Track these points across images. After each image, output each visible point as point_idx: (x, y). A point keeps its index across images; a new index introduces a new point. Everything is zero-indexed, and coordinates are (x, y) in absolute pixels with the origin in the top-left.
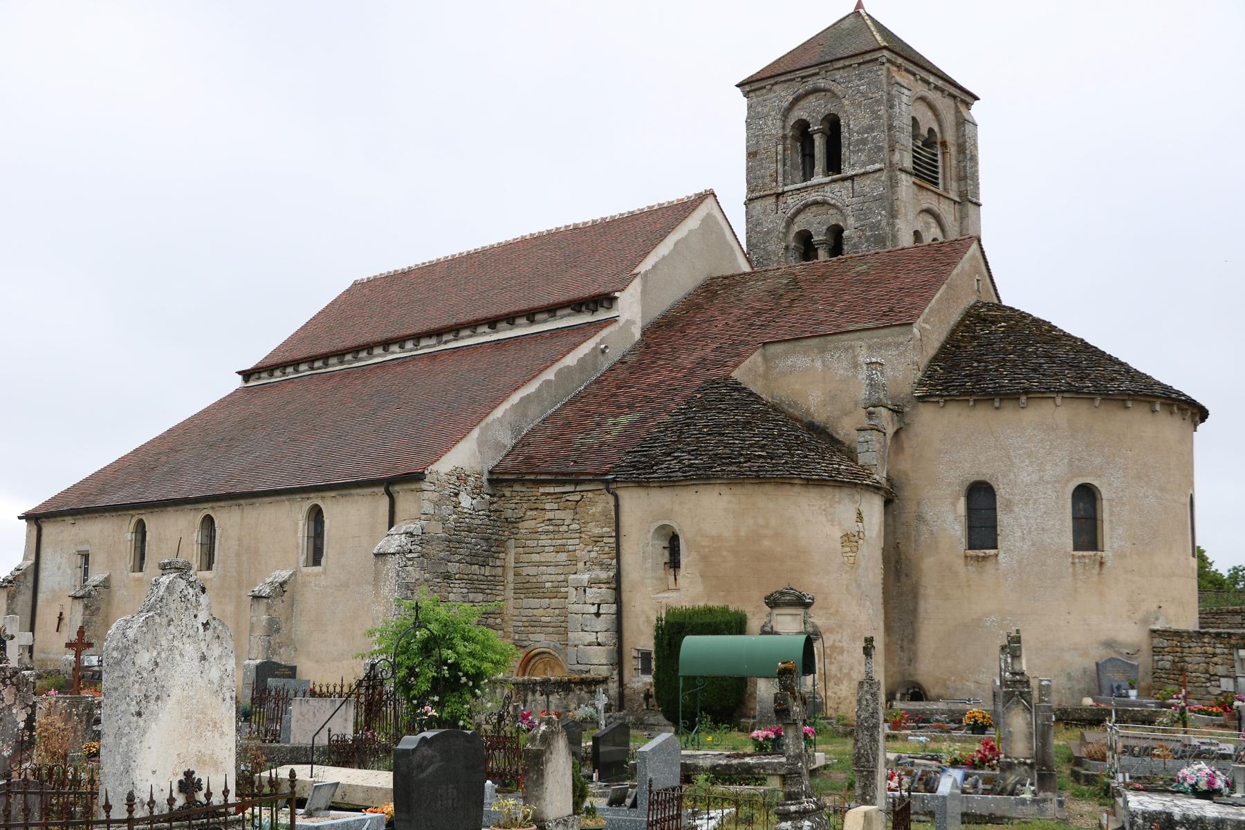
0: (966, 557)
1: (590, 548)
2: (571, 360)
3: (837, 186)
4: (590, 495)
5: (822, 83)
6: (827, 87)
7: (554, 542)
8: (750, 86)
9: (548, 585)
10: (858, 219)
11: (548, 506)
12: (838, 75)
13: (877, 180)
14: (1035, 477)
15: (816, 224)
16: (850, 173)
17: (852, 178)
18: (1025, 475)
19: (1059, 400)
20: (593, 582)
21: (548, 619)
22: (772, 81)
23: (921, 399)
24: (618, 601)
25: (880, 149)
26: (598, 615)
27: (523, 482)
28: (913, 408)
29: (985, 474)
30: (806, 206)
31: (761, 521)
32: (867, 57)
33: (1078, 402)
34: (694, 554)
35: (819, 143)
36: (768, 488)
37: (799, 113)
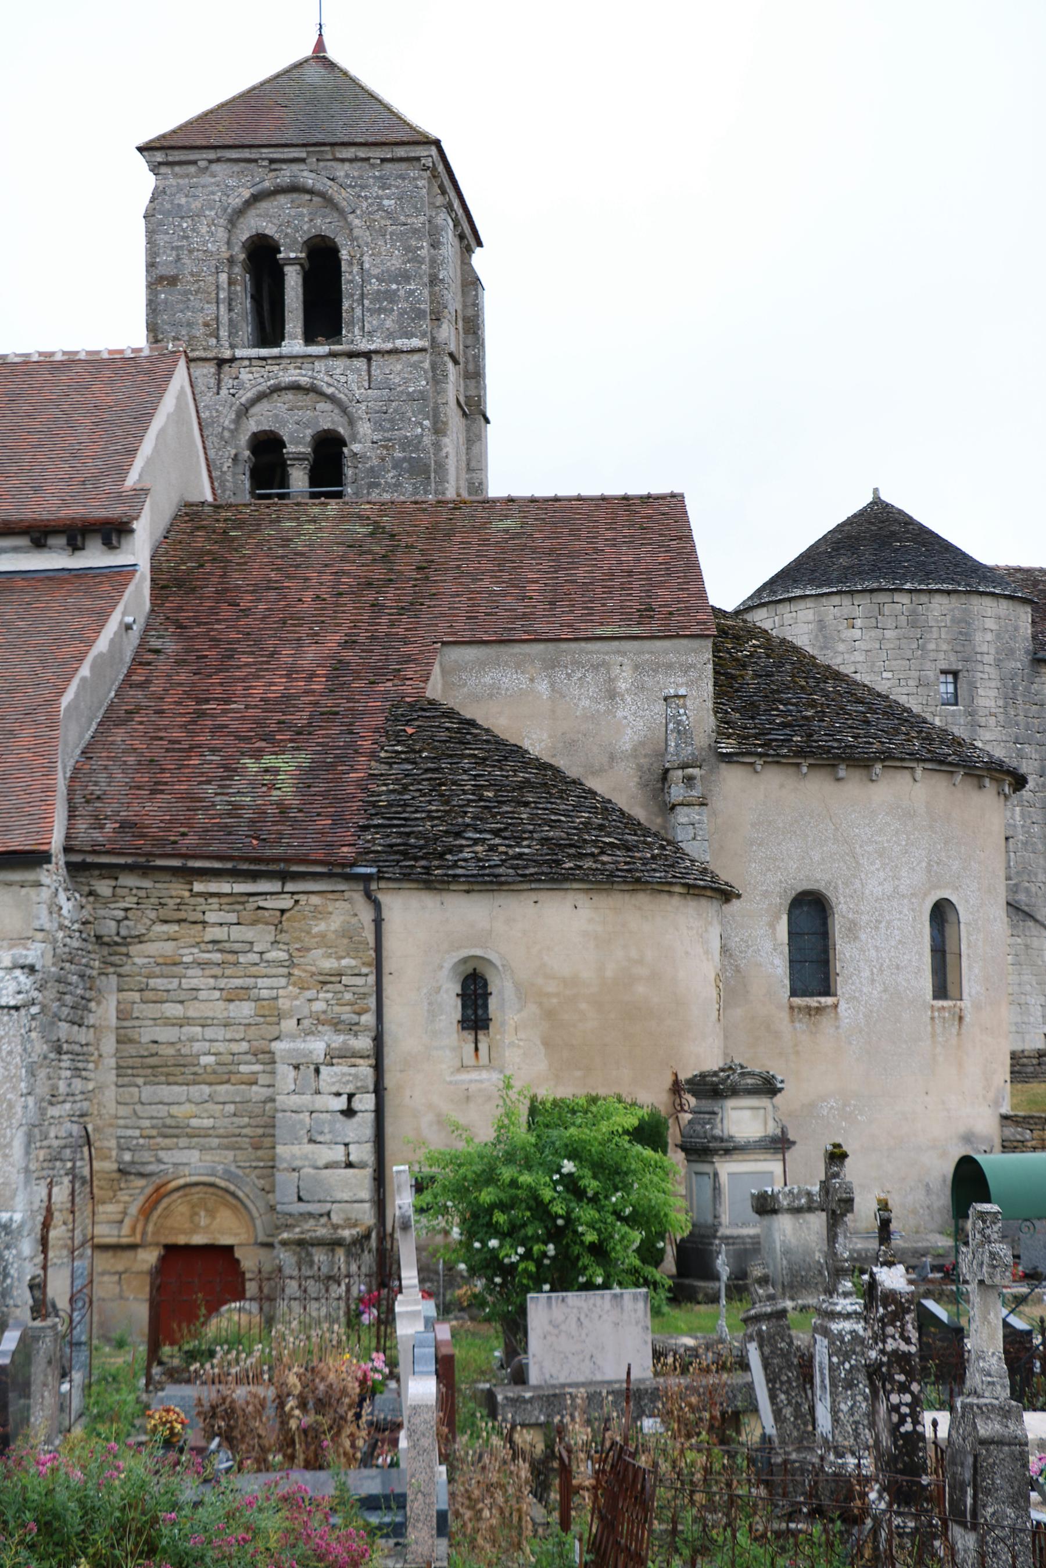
0: (792, 1008)
1: (310, 994)
2: (102, 644)
3: (340, 364)
4: (315, 900)
5: (309, 179)
6: (319, 187)
7: (222, 983)
8: (163, 152)
9: (205, 1060)
10: (378, 427)
11: (211, 917)
12: (341, 171)
13: (415, 366)
14: (888, 888)
15: (297, 428)
16: (364, 346)
17: (368, 355)
18: (875, 883)
19: (919, 772)
20: (332, 1057)
22: (212, 155)
23: (727, 758)
24: (379, 1090)
25: (420, 314)
26: (349, 1112)
27: (144, 870)
28: (711, 771)
29: (816, 879)
30: (277, 389)
31: (634, 954)
32: (401, 152)
33: (937, 775)
34: (532, 1008)
35: (293, 281)
36: (643, 899)
37: (256, 223)
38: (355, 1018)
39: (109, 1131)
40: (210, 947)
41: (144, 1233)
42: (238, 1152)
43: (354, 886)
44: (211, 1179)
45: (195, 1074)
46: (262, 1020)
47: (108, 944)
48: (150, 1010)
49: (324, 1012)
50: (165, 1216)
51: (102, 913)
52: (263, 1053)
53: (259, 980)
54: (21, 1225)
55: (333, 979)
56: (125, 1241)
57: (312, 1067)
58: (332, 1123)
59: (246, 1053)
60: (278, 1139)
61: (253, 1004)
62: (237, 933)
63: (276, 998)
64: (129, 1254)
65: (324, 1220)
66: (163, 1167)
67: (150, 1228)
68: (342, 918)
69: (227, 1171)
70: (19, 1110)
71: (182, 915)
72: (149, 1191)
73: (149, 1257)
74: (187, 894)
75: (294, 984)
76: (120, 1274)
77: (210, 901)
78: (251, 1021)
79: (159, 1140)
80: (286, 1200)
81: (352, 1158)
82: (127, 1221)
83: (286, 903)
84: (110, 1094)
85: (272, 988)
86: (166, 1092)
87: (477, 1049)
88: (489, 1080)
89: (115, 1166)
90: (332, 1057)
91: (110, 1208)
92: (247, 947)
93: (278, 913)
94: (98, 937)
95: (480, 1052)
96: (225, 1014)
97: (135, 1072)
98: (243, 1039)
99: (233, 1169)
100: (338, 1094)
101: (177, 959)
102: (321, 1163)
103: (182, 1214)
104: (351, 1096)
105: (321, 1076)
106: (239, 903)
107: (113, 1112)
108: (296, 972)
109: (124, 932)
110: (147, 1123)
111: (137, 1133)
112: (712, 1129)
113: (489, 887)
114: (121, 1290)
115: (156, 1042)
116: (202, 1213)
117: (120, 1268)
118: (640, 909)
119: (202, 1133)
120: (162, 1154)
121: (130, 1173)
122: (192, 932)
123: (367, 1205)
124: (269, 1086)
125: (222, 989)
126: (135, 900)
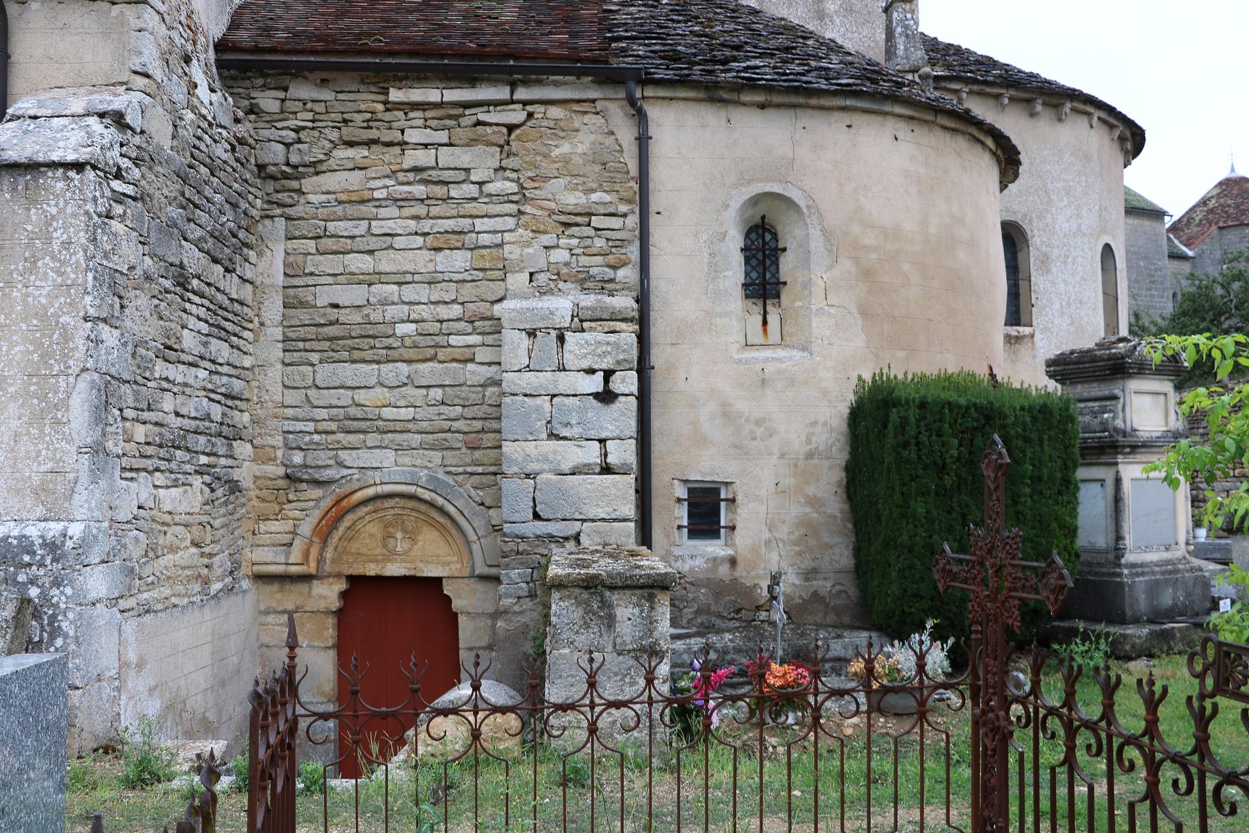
4: (555, 112)
7: (426, 226)
9: (402, 329)
11: (413, 136)
18: (1063, 221)
20: (581, 320)
21: (407, 413)
24: (643, 368)
26: (607, 396)
34: (846, 265)
38: (610, 273)
39: (273, 423)
40: (411, 176)
42: (447, 453)
43: (611, 93)
44: (411, 489)
45: (389, 348)
46: (481, 275)
47: (273, 178)
48: (330, 264)
49: (567, 264)
50: (349, 537)
51: (266, 133)
52: (483, 319)
53: (477, 221)
54: (85, 544)
55: (579, 219)
56: (294, 569)
57: (554, 333)
58: (582, 410)
59: (459, 320)
60: (504, 436)
61: (469, 254)
62: (447, 157)
63: (500, 246)
64: (302, 588)
65: (570, 545)
66: (345, 472)
67: (329, 554)
68: (592, 137)
69: (432, 479)
70: (80, 343)
71: (373, 134)
72: (326, 503)
73: (328, 594)
74: (380, 107)
75: (526, 227)
76: (290, 614)
77: (411, 115)
78: (466, 276)
79: (340, 436)
80: (516, 517)
81: (610, 459)
82: (297, 542)
83: (516, 115)
84: (275, 373)
85: (495, 232)
86: (348, 373)
87: (765, 323)
88: (790, 359)
89: (281, 471)
90: (581, 320)
91: (275, 526)
92: (461, 176)
93: (505, 130)
94: (261, 167)
95: (769, 327)
96: (431, 267)
97: (308, 345)
98: (453, 301)
99: (441, 476)
100: (591, 371)
101: (367, 194)
102: (566, 466)
103: (372, 536)
104: (608, 374)
105: (567, 346)
106: (450, 117)
107: (278, 398)
108: (528, 209)
109: (294, 159)
110: (323, 413)
111: (310, 427)
112: (1114, 418)
113: (793, 99)
115: (336, 306)
116: (399, 535)
117: (290, 607)
118: (959, 155)
119: (399, 426)
120: (343, 455)
121: (302, 481)
122: (387, 158)
123: (632, 525)
124: (490, 364)
125: (425, 234)
126: (310, 116)
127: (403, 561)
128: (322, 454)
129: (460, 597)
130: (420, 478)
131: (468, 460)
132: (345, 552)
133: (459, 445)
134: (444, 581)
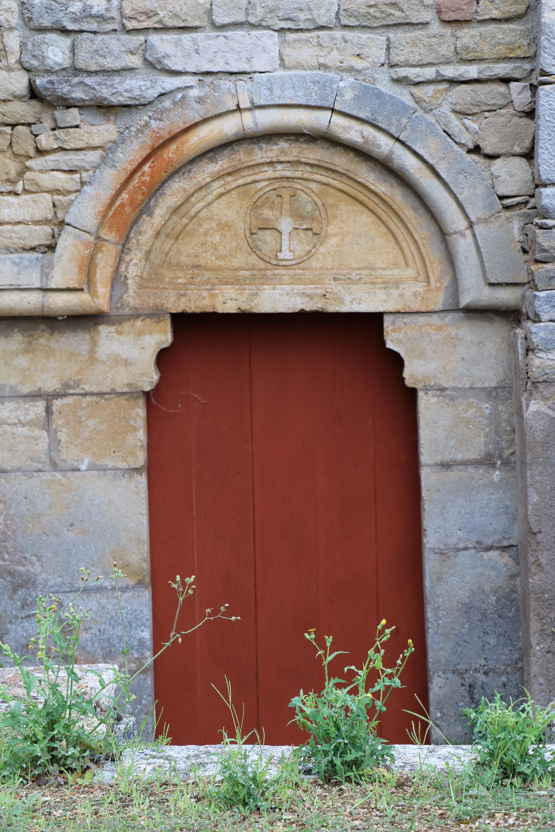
41: (117, 279)
42: (395, 35)
44: (318, 120)
56: (61, 302)
64: (75, 341)
66: (169, 83)
67: (134, 269)
69: (368, 93)
72: (131, 153)
73: (133, 354)
76: (49, 397)
82: (67, 242)
99: (385, 86)
103: (225, 226)
114: (55, 444)
116: (286, 224)
117: (50, 384)
121: (68, 104)
127: (296, 280)
128: (114, 43)
129: (421, 355)
130: (339, 93)
131: (446, 50)
132: (167, 263)
133: (427, 16)
134: (387, 321)
